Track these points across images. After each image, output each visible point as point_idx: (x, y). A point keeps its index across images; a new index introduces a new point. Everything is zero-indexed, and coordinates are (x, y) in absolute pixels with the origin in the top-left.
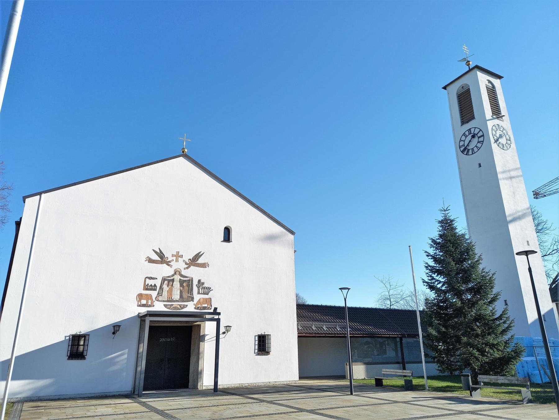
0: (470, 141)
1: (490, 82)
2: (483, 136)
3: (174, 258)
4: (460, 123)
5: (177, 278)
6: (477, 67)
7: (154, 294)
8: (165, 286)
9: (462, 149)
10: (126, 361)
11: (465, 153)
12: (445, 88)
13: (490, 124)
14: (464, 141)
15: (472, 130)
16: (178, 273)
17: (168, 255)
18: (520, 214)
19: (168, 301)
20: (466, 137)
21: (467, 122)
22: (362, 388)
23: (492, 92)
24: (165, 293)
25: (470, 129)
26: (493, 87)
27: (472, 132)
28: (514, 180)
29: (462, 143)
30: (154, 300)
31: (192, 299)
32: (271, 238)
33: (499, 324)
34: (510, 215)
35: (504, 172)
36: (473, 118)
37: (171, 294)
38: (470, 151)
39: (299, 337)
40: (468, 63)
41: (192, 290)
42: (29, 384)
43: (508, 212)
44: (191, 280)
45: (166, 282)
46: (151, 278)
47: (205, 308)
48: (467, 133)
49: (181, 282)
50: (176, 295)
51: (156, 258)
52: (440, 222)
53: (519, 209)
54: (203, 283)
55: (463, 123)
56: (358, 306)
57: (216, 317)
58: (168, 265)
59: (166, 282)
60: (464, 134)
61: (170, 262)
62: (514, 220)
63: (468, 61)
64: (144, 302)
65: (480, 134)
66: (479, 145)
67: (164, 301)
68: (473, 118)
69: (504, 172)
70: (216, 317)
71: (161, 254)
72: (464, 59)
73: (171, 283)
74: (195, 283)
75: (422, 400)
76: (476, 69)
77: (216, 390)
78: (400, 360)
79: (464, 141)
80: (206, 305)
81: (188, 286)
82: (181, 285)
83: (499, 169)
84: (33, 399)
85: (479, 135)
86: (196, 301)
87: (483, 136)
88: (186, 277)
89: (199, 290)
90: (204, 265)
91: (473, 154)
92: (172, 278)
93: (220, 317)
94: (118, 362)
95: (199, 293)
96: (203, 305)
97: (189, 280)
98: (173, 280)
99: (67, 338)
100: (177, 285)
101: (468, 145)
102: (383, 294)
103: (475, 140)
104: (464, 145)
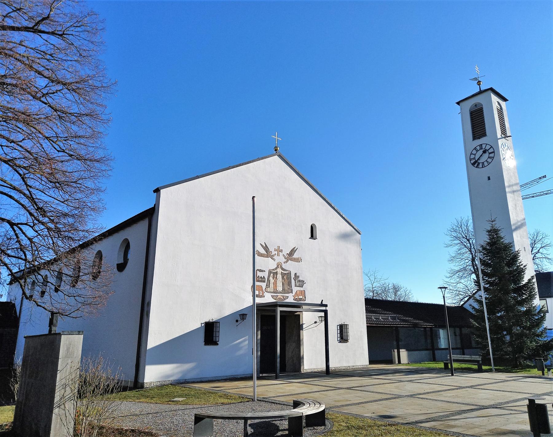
0: (481, 156)
1: (499, 103)
2: (494, 152)
3: (276, 252)
5: (279, 270)
6: (492, 89)
8: (271, 278)
9: (472, 162)
10: (245, 346)
11: (476, 166)
12: (458, 103)
13: (500, 142)
14: (475, 155)
15: (484, 146)
16: (279, 266)
17: (271, 249)
18: (519, 223)
19: (274, 292)
20: (477, 151)
21: (479, 138)
23: (500, 111)
24: (272, 285)
25: (481, 145)
26: (501, 108)
27: (484, 148)
28: (515, 193)
29: (473, 156)
32: (345, 236)
34: (514, 225)
35: (509, 186)
36: (484, 135)
37: (276, 286)
38: (481, 165)
39: (367, 326)
40: (479, 83)
41: (291, 282)
42: (177, 367)
43: (513, 222)
45: (272, 274)
47: (301, 300)
48: (478, 148)
50: (280, 288)
52: (489, 231)
53: (519, 219)
54: (298, 277)
55: (474, 138)
56: (426, 302)
57: (324, 308)
59: (272, 274)
60: (475, 148)
62: (516, 229)
63: (479, 82)
66: (489, 160)
67: (271, 292)
68: (484, 135)
69: (509, 186)
70: (324, 308)
72: (475, 79)
74: (293, 276)
75: (511, 380)
76: (490, 91)
77: (328, 373)
78: (429, 347)
79: (475, 155)
80: (301, 297)
81: (287, 278)
82: (283, 278)
83: (506, 184)
84: (182, 381)
85: (490, 151)
87: (494, 152)
88: (286, 271)
89: (295, 282)
90: (298, 260)
94: (242, 347)
95: (296, 286)
96: (300, 297)
97: (288, 273)
99: (203, 325)
100: (279, 276)
101: (479, 159)
102: (367, 286)
103: (486, 156)
104: (474, 158)
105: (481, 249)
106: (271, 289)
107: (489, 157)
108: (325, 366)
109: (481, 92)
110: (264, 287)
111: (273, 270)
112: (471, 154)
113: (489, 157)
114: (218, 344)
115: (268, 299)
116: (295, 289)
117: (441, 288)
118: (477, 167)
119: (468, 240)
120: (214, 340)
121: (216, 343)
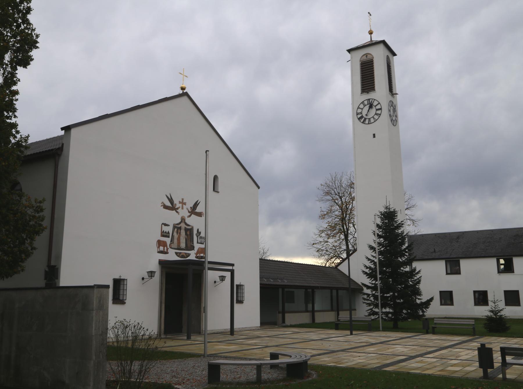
2: (381, 109)
3: (181, 205)
6: (384, 42)
7: (168, 240)
8: (175, 234)
9: (359, 116)
11: (362, 121)
12: (349, 51)
16: (183, 221)
17: (176, 201)
20: (365, 106)
22: (369, 327)
24: (176, 241)
30: (168, 247)
31: (192, 248)
44: (191, 230)
45: (176, 229)
46: (166, 225)
47: (202, 257)
49: (186, 230)
50: (183, 245)
51: (168, 204)
58: (177, 212)
59: (176, 229)
64: (161, 248)
65: (378, 107)
71: (171, 200)
74: (195, 232)
82: (186, 234)
86: (196, 249)
87: (381, 109)
88: (189, 225)
91: (369, 124)
92: (179, 226)
93: (234, 268)
95: (198, 243)
97: (191, 229)
98: (180, 228)
100: (183, 232)
103: (373, 111)
105: (379, 214)
106: (175, 245)
107: (376, 114)
108: (229, 327)
109: (372, 44)
111: (178, 224)
112: (358, 108)
113: (376, 114)
114: (125, 303)
115: (172, 256)
116: (197, 246)
118: (363, 123)
119: (341, 198)
120: (121, 298)
121: (123, 302)
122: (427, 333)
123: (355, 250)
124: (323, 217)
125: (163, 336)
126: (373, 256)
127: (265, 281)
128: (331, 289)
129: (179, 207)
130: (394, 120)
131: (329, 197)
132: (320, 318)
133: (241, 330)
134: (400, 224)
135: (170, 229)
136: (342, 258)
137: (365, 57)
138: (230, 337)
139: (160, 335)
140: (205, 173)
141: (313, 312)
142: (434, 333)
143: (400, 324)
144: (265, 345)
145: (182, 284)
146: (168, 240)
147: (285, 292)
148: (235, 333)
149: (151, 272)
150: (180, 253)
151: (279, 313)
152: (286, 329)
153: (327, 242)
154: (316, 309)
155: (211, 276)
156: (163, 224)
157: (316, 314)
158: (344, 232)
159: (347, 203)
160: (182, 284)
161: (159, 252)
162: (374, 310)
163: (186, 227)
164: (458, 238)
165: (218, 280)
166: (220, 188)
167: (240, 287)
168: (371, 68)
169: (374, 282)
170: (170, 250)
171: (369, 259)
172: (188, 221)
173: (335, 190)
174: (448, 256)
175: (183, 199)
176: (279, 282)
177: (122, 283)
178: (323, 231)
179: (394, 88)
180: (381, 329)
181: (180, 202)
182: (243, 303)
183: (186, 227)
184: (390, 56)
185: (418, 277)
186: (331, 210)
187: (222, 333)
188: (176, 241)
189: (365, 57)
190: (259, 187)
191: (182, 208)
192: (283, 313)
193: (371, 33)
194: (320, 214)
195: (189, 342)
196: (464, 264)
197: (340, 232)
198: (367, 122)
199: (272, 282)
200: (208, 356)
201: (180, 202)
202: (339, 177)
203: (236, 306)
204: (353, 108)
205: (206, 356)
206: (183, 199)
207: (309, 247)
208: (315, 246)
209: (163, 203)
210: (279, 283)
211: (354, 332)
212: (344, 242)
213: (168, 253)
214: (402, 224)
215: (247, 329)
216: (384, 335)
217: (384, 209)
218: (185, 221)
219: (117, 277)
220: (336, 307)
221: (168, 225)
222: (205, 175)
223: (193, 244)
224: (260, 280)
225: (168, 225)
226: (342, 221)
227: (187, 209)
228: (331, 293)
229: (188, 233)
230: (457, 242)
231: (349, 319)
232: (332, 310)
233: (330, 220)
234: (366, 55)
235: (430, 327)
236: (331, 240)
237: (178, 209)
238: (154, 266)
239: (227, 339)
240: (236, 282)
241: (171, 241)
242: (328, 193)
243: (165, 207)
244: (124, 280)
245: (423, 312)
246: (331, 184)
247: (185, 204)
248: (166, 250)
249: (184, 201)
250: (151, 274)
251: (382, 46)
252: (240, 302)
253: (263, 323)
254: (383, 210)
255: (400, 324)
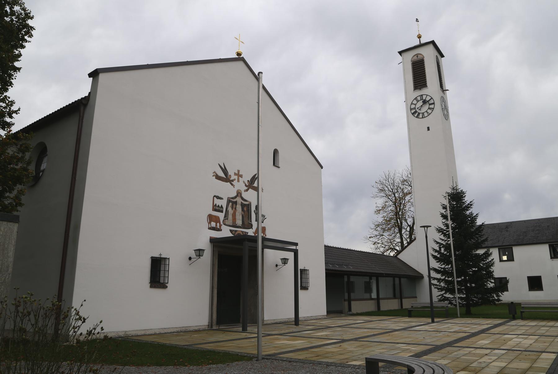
3: (236, 177)
4: (413, 89)
8: (230, 209)
9: (413, 111)
11: (416, 115)
12: (400, 53)
15: (424, 97)
16: (239, 195)
17: (231, 172)
20: (418, 101)
22: (432, 313)
24: (230, 217)
27: (424, 98)
30: (222, 223)
31: (250, 226)
33: (17, 198)
44: (249, 206)
45: (231, 204)
46: (218, 198)
49: (243, 205)
50: (239, 222)
51: (221, 174)
57: (294, 247)
58: (232, 184)
59: (231, 204)
60: (416, 99)
61: (233, 181)
64: (213, 224)
65: (432, 102)
66: (429, 111)
70: (294, 247)
71: (225, 171)
73: (234, 205)
74: (253, 208)
82: (243, 210)
87: (434, 103)
88: (246, 201)
92: (235, 200)
97: (248, 205)
100: (239, 208)
103: (426, 107)
104: (415, 108)
106: (230, 221)
107: (429, 108)
109: (421, 45)
110: (222, 219)
111: (232, 198)
112: (412, 103)
113: (429, 108)
114: (167, 287)
115: (226, 232)
117: (424, 227)
118: (417, 117)
120: (162, 281)
121: (163, 286)
122: (514, 318)
123: (411, 241)
124: (378, 212)
125: (214, 328)
126: (441, 239)
127: (331, 267)
128: (394, 276)
129: (235, 180)
130: (446, 116)
131: (383, 194)
132: (386, 305)
133: (306, 320)
134: (468, 204)
135: (223, 203)
136: (396, 250)
137: (416, 57)
138: (294, 328)
139: (212, 326)
140: (257, 101)
141: (378, 299)
142: (523, 318)
143: (473, 310)
144: (340, 338)
145: (236, 264)
146: (221, 216)
147: (351, 280)
148: (300, 323)
149: (199, 250)
150: (236, 231)
151: (345, 300)
152: (355, 318)
153: (383, 235)
154: (381, 297)
155: (272, 256)
156: (214, 196)
157: (382, 302)
158: (398, 226)
159: (403, 198)
160: (236, 264)
161: (210, 228)
162: (444, 295)
163: (243, 202)
164: (507, 227)
165: (280, 263)
166: (281, 163)
167: (304, 272)
168: (421, 69)
169: (443, 266)
170: (223, 227)
171: (437, 243)
172: (245, 195)
173: (389, 187)
174: (500, 244)
175: (239, 171)
176: (345, 268)
177: (163, 262)
178: (378, 225)
179: (444, 86)
180: (459, 315)
181: (235, 174)
182: (308, 289)
183: (243, 202)
184: (439, 57)
185: (490, 259)
186: (386, 205)
187: (285, 323)
188: (230, 217)
189: (415, 58)
190: (322, 167)
191: (238, 181)
192: (349, 301)
193: (419, 37)
194: (375, 209)
195: (244, 335)
196: (517, 251)
197: (395, 226)
198: (421, 116)
199: (337, 268)
200: (263, 358)
201: (235, 174)
202: (392, 175)
203: (301, 293)
204: (407, 104)
205: (260, 358)
206: (239, 171)
207: (366, 241)
208: (371, 239)
209: (215, 172)
210: (345, 269)
211: (436, 320)
212: (398, 235)
213: (221, 230)
214: (471, 205)
215: (313, 318)
216: (469, 322)
217: (451, 190)
218: (241, 195)
219: (156, 255)
220: (398, 294)
221: (221, 199)
222: (260, 124)
223: (251, 221)
224: (326, 266)
225: (221, 199)
226: (396, 215)
227: (244, 182)
228: (394, 281)
229: (245, 209)
230: (507, 231)
231: (430, 305)
232: (395, 297)
233: (385, 214)
234: (417, 55)
235: (515, 312)
236: (386, 234)
237: (233, 181)
238: (204, 243)
239: (291, 330)
240: (300, 267)
241: (225, 217)
242: (382, 190)
243: (218, 177)
244: (165, 259)
245: (498, 296)
246: (384, 181)
247: (241, 176)
248: (218, 227)
249: (240, 173)
250: (199, 252)
251: (431, 46)
252: (305, 288)
253: (328, 312)
254: (450, 191)
255: (473, 310)
